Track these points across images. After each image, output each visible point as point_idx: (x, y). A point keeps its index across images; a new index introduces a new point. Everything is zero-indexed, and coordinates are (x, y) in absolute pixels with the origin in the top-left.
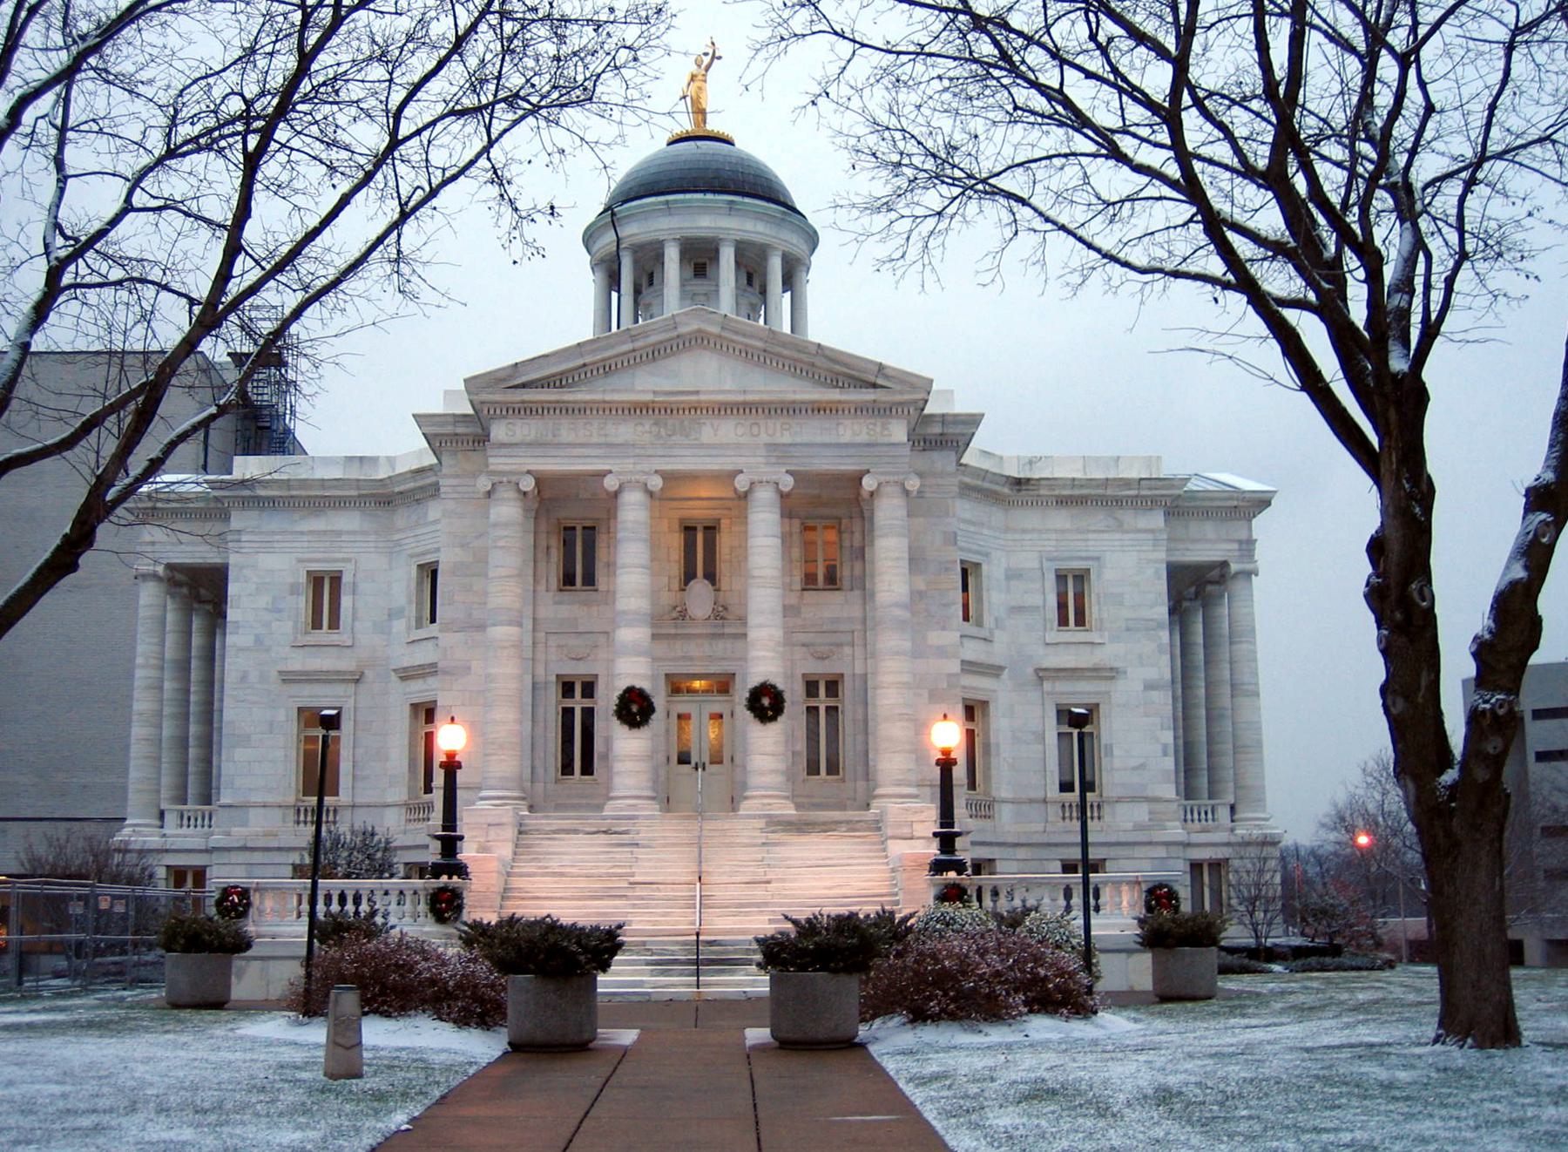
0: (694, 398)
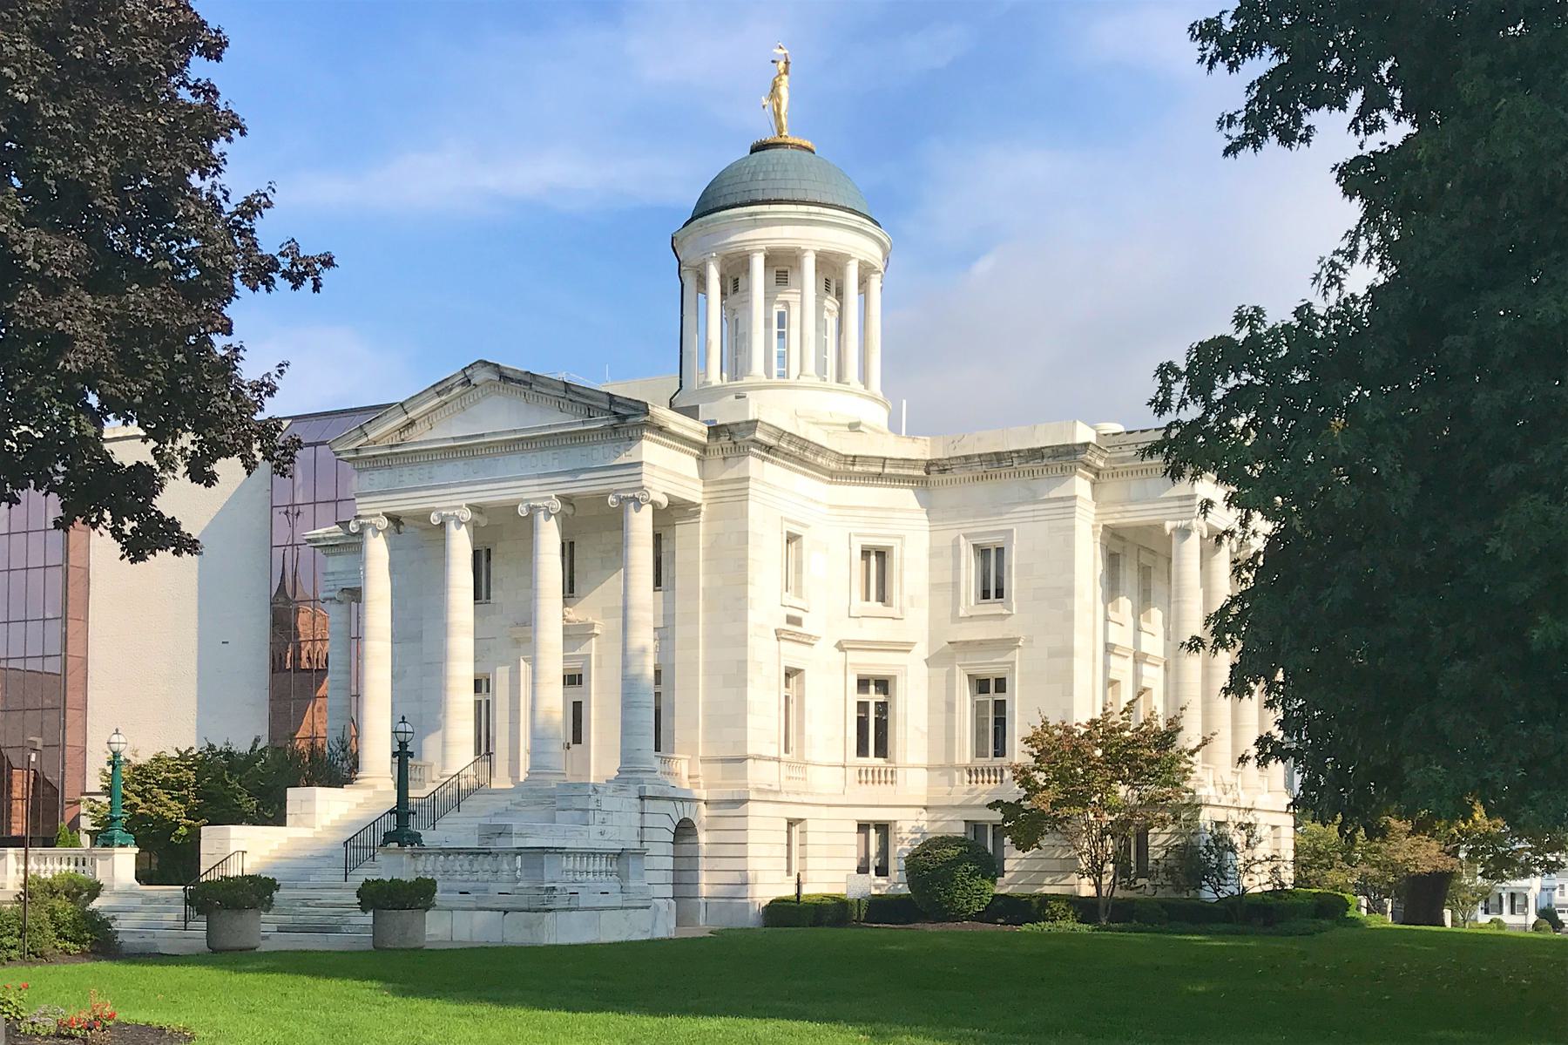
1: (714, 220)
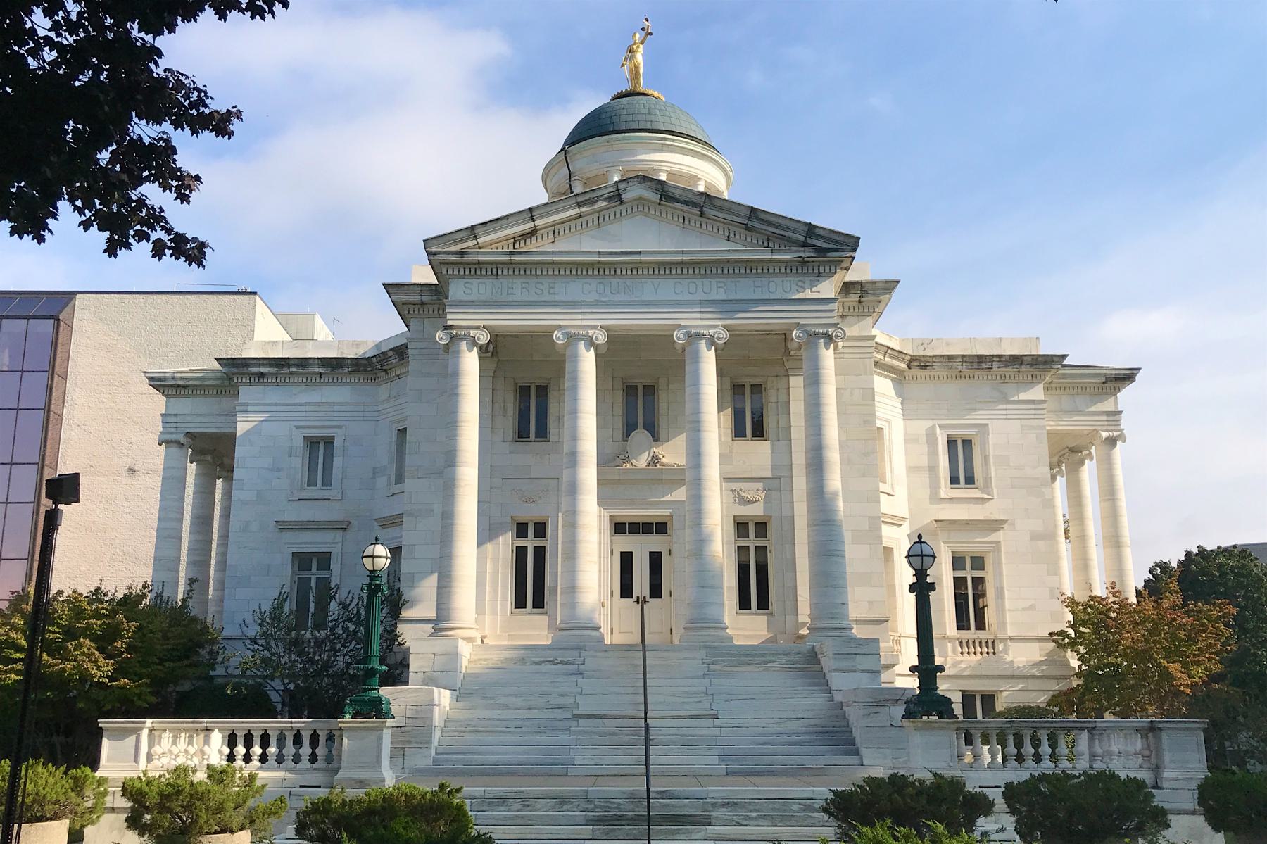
0: (637, 258)
1: (624, 139)
